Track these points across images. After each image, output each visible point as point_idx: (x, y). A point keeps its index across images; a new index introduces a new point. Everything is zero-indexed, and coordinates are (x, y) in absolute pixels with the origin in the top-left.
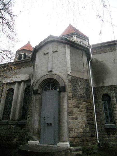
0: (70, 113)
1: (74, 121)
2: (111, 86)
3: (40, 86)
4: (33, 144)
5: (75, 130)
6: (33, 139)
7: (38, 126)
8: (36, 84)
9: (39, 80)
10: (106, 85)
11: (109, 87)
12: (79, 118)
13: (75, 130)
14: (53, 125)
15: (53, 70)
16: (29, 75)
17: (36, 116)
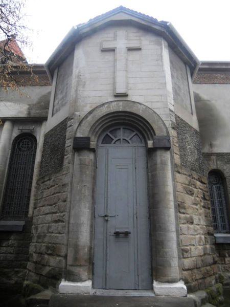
0: (180, 207)
1: (188, 227)
2: (227, 153)
3: (93, 128)
4: (79, 292)
5: (190, 248)
6: (72, 277)
7: (88, 238)
8: (84, 122)
9: (90, 113)
10: (216, 150)
11: (222, 155)
12: (196, 219)
13: (191, 250)
14: (131, 236)
15: (129, 93)
16: (28, 107)
17: (85, 210)
